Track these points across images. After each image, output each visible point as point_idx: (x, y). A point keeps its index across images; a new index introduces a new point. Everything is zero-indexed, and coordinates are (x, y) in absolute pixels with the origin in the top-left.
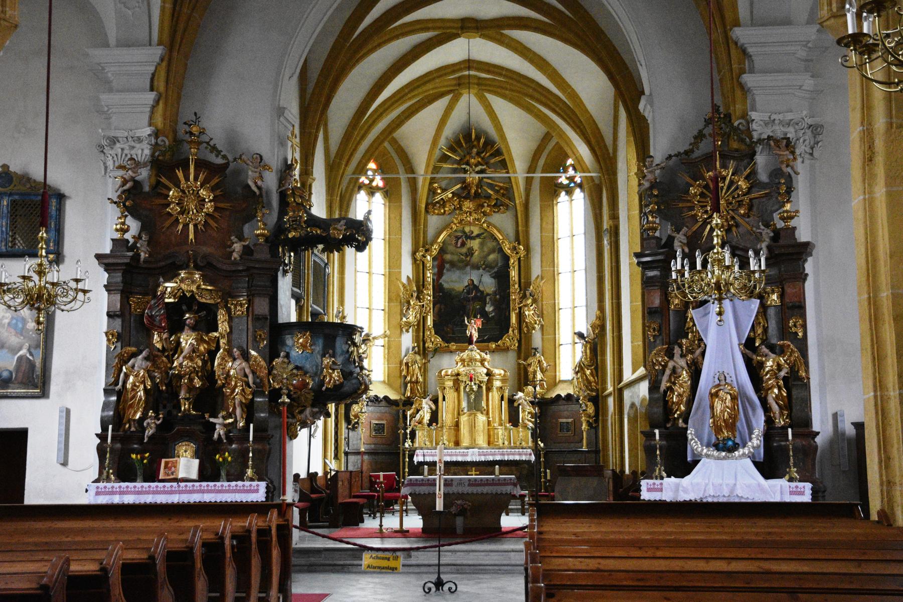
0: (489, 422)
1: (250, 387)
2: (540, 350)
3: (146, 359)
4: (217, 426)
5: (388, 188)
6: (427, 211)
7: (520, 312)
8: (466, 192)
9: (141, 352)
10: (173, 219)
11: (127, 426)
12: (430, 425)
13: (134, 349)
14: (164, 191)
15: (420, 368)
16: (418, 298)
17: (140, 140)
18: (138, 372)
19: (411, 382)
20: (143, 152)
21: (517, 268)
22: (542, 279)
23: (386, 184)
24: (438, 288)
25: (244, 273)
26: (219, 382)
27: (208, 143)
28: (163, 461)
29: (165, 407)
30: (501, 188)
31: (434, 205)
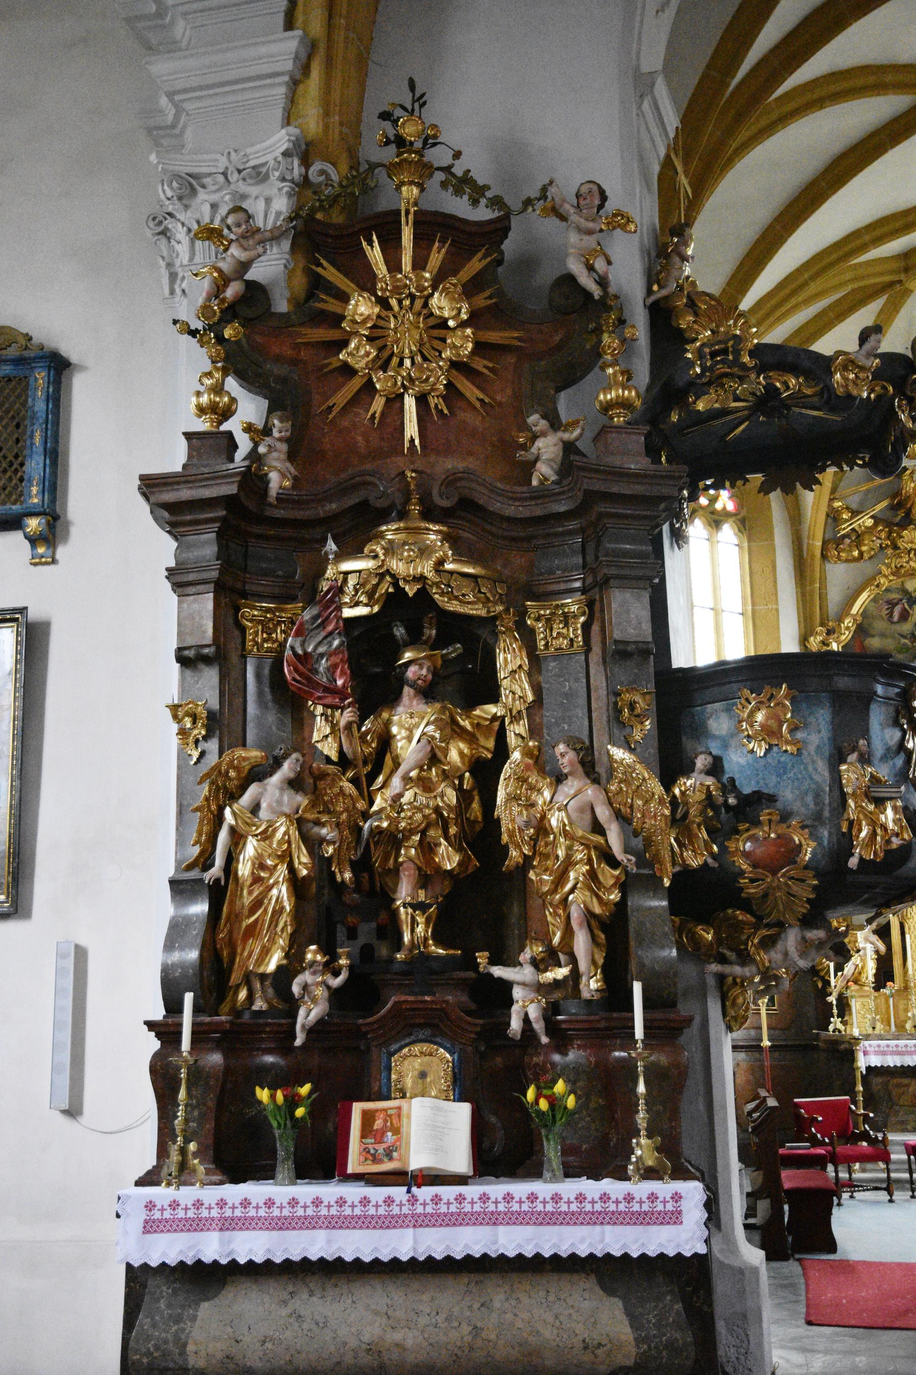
1: (613, 862)
3: (294, 784)
4: (518, 993)
5: (744, 513)
6: (824, 557)
8: (901, 514)
9: (277, 763)
10: (356, 383)
11: (243, 994)
13: (255, 754)
14: (332, 305)
17: (259, 175)
18: (271, 824)
20: (272, 205)
23: (740, 505)
25: (573, 525)
26: (514, 853)
27: (447, 169)
28: (357, 1108)
29: (352, 934)
31: (839, 541)
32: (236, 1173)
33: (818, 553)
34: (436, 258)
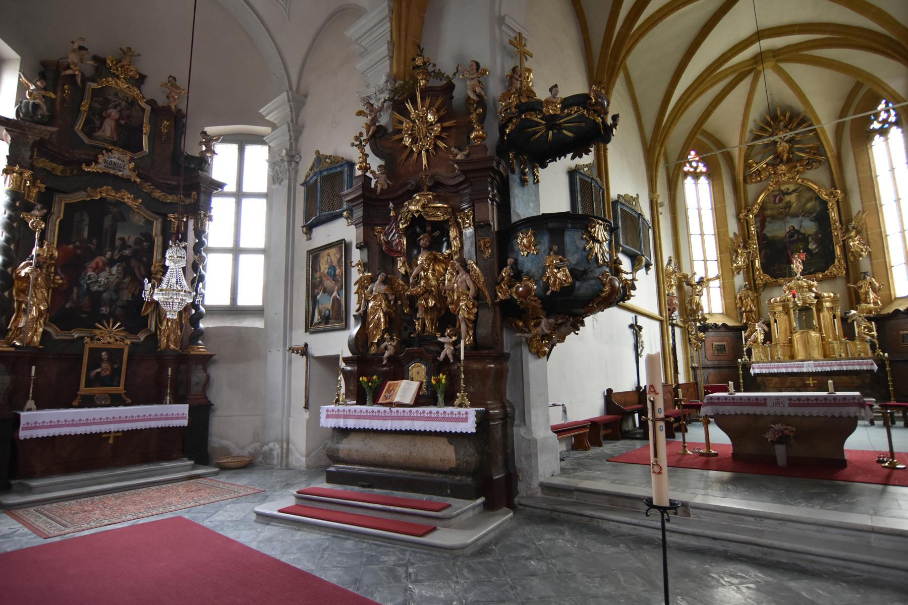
0: (823, 339)
2: (870, 273)
7: (844, 244)
8: (779, 160)
10: (408, 151)
12: (764, 343)
15: (753, 301)
16: (745, 247)
19: (745, 311)
21: (836, 209)
22: (864, 212)
24: (761, 237)
30: (811, 148)
32: (361, 401)
33: (742, 181)
34: (428, 102)
